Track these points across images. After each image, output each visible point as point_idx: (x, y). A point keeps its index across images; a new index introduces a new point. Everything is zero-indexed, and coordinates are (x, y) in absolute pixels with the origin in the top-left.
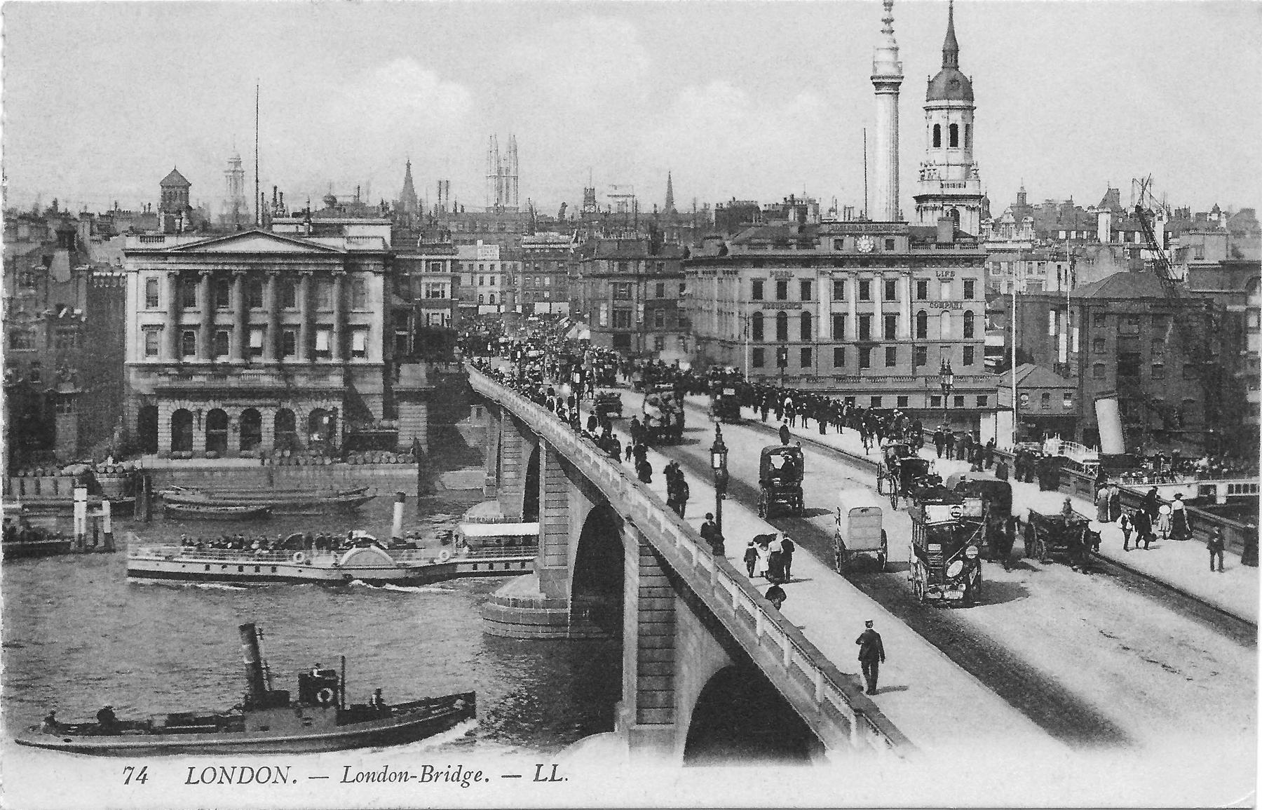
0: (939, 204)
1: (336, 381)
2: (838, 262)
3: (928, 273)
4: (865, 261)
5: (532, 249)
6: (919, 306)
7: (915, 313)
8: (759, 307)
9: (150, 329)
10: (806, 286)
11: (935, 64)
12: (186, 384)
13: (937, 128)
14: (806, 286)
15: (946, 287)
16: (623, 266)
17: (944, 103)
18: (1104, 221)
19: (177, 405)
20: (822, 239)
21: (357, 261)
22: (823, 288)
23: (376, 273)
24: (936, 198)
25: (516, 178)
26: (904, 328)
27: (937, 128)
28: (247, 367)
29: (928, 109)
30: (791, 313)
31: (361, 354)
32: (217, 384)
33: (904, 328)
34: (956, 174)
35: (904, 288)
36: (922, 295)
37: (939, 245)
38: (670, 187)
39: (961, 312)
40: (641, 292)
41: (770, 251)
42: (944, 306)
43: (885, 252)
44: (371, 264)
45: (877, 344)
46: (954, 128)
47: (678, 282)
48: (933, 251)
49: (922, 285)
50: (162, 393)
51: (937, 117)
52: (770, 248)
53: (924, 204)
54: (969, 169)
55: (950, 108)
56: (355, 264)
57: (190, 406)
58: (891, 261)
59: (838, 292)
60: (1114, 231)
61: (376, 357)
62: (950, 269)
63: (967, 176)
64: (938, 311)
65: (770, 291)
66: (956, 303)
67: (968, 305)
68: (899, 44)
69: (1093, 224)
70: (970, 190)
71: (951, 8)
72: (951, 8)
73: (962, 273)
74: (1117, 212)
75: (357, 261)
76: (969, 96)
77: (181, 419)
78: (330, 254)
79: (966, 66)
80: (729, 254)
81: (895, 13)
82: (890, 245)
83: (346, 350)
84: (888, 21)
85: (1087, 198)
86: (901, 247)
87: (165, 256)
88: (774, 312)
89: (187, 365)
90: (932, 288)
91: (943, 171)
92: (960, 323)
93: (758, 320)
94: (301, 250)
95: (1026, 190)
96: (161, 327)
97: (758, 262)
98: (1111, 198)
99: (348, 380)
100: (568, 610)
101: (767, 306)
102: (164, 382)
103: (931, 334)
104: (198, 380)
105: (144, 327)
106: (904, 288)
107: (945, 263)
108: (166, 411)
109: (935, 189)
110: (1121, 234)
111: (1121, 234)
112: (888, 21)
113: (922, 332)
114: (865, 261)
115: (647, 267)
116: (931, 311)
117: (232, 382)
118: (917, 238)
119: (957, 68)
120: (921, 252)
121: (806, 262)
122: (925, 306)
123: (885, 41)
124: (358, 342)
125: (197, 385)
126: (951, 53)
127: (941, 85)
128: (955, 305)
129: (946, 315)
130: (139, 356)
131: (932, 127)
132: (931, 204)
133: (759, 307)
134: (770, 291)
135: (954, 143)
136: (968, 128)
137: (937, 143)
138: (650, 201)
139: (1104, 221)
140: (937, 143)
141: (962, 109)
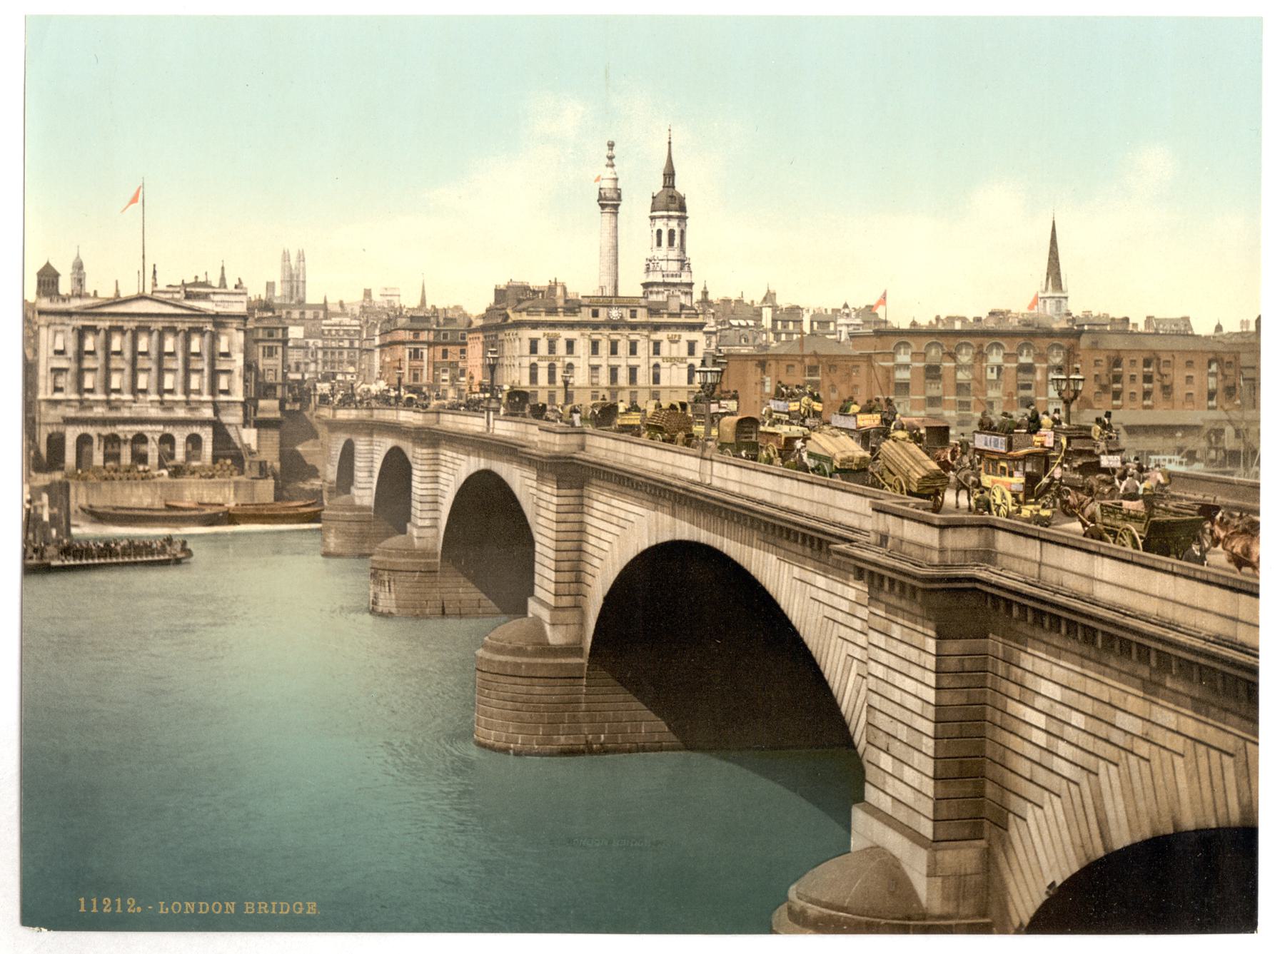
0: (661, 289)
1: (208, 413)
2: (596, 326)
3: (661, 335)
4: (614, 325)
5: (330, 330)
6: (653, 361)
7: (651, 365)
8: (534, 360)
9: (57, 371)
10: (570, 344)
11: (657, 186)
12: (89, 414)
13: (659, 232)
14: (570, 344)
15: (674, 346)
16: (416, 335)
17: (665, 213)
18: (767, 314)
19: (81, 430)
20: (583, 309)
21: (224, 320)
22: (582, 346)
23: (238, 330)
24: (658, 284)
25: (304, 282)
26: (643, 378)
27: (659, 232)
28: (135, 402)
29: (652, 218)
30: (559, 364)
31: (226, 392)
32: (113, 414)
33: (643, 378)
34: (674, 266)
35: (644, 348)
36: (657, 352)
37: (671, 315)
38: (423, 291)
39: (686, 365)
40: (431, 355)
41: (543, 317)
42: (673, 360)
43: (630, 320)
44: (235, 323)
45: (622, 389)
46: (671, 233)
47: (459, 348)
48: (665, 319)
49: (657, 344)
50: (69, 421)
51: (660, 224)
52: (543, 314)
53: (650, 289)
54: (683, 263)
55: (669, 217)
56: (223, 323)
57: (91, 431)
58: (633, 327)
59: (595, 346)
60: (774, 321)
61: (238, 396)
62: (677, 333)
63: (682, 269)
64: (668, 364)
65: (543, 348)
66: (682, 358)
67: (690, 361)
68: (619, 176)
69: (758, 315)
70: (685, 278)
71: (670, 143)
72: (670, 143)
73: (686, 336)
74: (775, 308)
75: (224, 320)
76: (682, 208)
77: (84, 441)
78: (203, 315)
79: (681, 187)
80: (510, 321)
81: (616, 151)
82: (633, 314)
83: (214, 389)
84: (611, 158)
85: (754, 296)
86: (642, 316)
87: (69, 314)
88: (546, 364)
89: (87, 400)
90: (665, 349)
91: (663, 265)
92: (685, 373)
93: (534, 367)
94: (185, 312)
95: (708, 289)
96: (66, 370)
97: (535, 325)
98: (769, 297)
99: (216, 412)
100: (439, 560)
101: (542, 359)
102: (71, 413)
103: (664, 381)
104: (99, 411)
105: (53, 370)
106: (644, 348)
107: (673, 328)
108: (72, 434)
109: (659, 279)
110: (779, 323)
111: (779, 323)
112: (611, 158)
113: (656, 379)
114: (614, 325)
115: (435, 337)
116: (663, 365)
117: (126, 413)
118: (653, 310)
119: (674, 187)
120: (656, 320)
121: (571, 326)
122: (659, 361)
123: (608, 173)
124: (223, 383)
125: (99, 415)
126: (670, 175)
127: (663, 198)
128: (682, 360)
129: (674, 367)
130: (49, 391)
131: (655, 232)
132: (655, 289)
133: (534, 360)
134: (543, 348)
135: (671, 243)
136: (682, 233)
137: (659, 244)
138: (409, 301)
139: (767, 314)
140: (659, 244)
141: (678, 217)
